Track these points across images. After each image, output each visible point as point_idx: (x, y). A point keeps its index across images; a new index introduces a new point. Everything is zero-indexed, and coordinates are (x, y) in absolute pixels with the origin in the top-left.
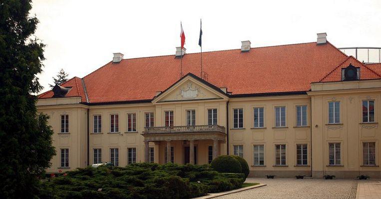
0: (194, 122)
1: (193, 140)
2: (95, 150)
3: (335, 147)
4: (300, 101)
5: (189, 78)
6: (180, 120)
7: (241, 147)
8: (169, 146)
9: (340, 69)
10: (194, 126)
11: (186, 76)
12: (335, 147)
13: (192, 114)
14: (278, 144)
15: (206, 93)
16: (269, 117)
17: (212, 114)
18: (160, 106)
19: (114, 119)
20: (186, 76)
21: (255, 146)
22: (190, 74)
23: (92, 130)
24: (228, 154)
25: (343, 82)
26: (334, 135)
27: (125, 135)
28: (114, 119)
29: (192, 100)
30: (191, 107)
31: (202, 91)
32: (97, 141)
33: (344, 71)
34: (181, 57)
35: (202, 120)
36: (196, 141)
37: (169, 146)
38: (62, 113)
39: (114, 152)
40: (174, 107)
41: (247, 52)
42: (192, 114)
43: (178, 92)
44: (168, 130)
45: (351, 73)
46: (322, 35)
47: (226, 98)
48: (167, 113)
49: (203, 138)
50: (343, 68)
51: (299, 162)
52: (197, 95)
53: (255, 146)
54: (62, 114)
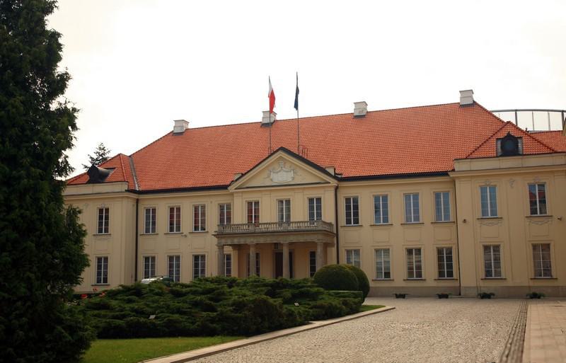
2: (147, 259)
3: (492, 252)
4: (439, 185)
5: (281, 154)
6: (268, 214)
7: (357, 252)
8: (252, 252)
9: (493, 140)
11: (277, 151)
15: (305, 175)
17: (315, 205)
19: (174, 213)
20: (277, 151)
21: (377, 251)
22: (282, 149)
23: (142, 229)
24: (338, 262)
25: (501, 158)
26: (490, 233)
27: (189, 236)
28: (174, 213)
30: (284, 195)
32: (149, 245)
33: (499, 142)
35: (300, 213)
37: (252, 252)
38: (100, 205)
39: (174, 261)
41: (362, 117)
42: (285, 205)
44: (252, 228)
45: (509, 145)
46: (467, 93)
47: (334, 182)
48: (250, 204)
49: (301, 239)
50: (497, 139)
52: (293, 178)
53: (377, 251)
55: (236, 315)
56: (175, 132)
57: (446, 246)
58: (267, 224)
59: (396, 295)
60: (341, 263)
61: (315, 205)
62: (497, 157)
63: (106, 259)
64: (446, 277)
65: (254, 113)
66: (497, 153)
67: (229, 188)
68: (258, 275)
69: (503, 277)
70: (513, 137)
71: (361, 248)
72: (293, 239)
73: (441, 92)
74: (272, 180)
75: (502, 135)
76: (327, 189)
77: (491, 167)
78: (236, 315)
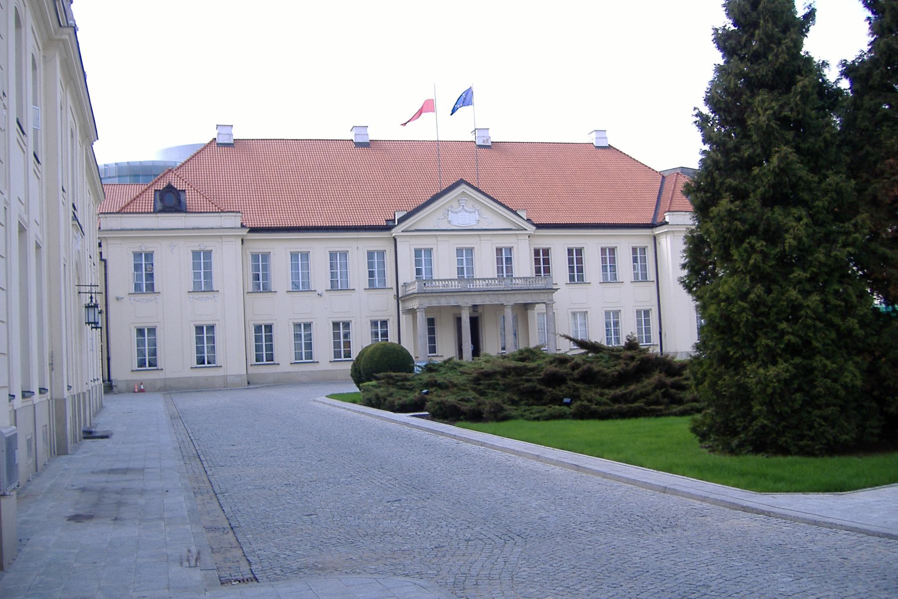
0: (471, 270)
1: (512, 303)
3: (205, 333)
4: (640, 238)
6: (445, 268)
12: (205, 333)
13: (466, 254)
14: (259, 323)
15: (493, 218)
16: (280, 271)
17: (504, 258)
18: (408, 239)
19: (576, 257)
21: (574, 314)
25: (159, 215)
26: (205, 310)
27: (325, 293)
28: (576, 257)
29: (469, 230)
30: (465, 242)
31: (487, 214)
33: (158, 194)
35: (485, 267)
38: (137, 246)
40: (477, 239)
42: (466, 254)
44: (540, 284)
45: (171, 200)
46: (601, 132)
48: (137, 255)
49: (444, 302)
50: (156, 191)
51: (298, 356)
53: (574, 314)
55: (542, 387)
57: (148, 325)
58: (445, 280)
59: (10, 401)
61: (504, 258)
62: (154, 212)
63: (269, 328)
64: (147, 367)
66: (154, 209)
67: (393, 230)
68: (433, 350)
70: (176, 189)
75: (161, 186)
76: (439, 239)
77: (210, 225)
78: (542, 387)
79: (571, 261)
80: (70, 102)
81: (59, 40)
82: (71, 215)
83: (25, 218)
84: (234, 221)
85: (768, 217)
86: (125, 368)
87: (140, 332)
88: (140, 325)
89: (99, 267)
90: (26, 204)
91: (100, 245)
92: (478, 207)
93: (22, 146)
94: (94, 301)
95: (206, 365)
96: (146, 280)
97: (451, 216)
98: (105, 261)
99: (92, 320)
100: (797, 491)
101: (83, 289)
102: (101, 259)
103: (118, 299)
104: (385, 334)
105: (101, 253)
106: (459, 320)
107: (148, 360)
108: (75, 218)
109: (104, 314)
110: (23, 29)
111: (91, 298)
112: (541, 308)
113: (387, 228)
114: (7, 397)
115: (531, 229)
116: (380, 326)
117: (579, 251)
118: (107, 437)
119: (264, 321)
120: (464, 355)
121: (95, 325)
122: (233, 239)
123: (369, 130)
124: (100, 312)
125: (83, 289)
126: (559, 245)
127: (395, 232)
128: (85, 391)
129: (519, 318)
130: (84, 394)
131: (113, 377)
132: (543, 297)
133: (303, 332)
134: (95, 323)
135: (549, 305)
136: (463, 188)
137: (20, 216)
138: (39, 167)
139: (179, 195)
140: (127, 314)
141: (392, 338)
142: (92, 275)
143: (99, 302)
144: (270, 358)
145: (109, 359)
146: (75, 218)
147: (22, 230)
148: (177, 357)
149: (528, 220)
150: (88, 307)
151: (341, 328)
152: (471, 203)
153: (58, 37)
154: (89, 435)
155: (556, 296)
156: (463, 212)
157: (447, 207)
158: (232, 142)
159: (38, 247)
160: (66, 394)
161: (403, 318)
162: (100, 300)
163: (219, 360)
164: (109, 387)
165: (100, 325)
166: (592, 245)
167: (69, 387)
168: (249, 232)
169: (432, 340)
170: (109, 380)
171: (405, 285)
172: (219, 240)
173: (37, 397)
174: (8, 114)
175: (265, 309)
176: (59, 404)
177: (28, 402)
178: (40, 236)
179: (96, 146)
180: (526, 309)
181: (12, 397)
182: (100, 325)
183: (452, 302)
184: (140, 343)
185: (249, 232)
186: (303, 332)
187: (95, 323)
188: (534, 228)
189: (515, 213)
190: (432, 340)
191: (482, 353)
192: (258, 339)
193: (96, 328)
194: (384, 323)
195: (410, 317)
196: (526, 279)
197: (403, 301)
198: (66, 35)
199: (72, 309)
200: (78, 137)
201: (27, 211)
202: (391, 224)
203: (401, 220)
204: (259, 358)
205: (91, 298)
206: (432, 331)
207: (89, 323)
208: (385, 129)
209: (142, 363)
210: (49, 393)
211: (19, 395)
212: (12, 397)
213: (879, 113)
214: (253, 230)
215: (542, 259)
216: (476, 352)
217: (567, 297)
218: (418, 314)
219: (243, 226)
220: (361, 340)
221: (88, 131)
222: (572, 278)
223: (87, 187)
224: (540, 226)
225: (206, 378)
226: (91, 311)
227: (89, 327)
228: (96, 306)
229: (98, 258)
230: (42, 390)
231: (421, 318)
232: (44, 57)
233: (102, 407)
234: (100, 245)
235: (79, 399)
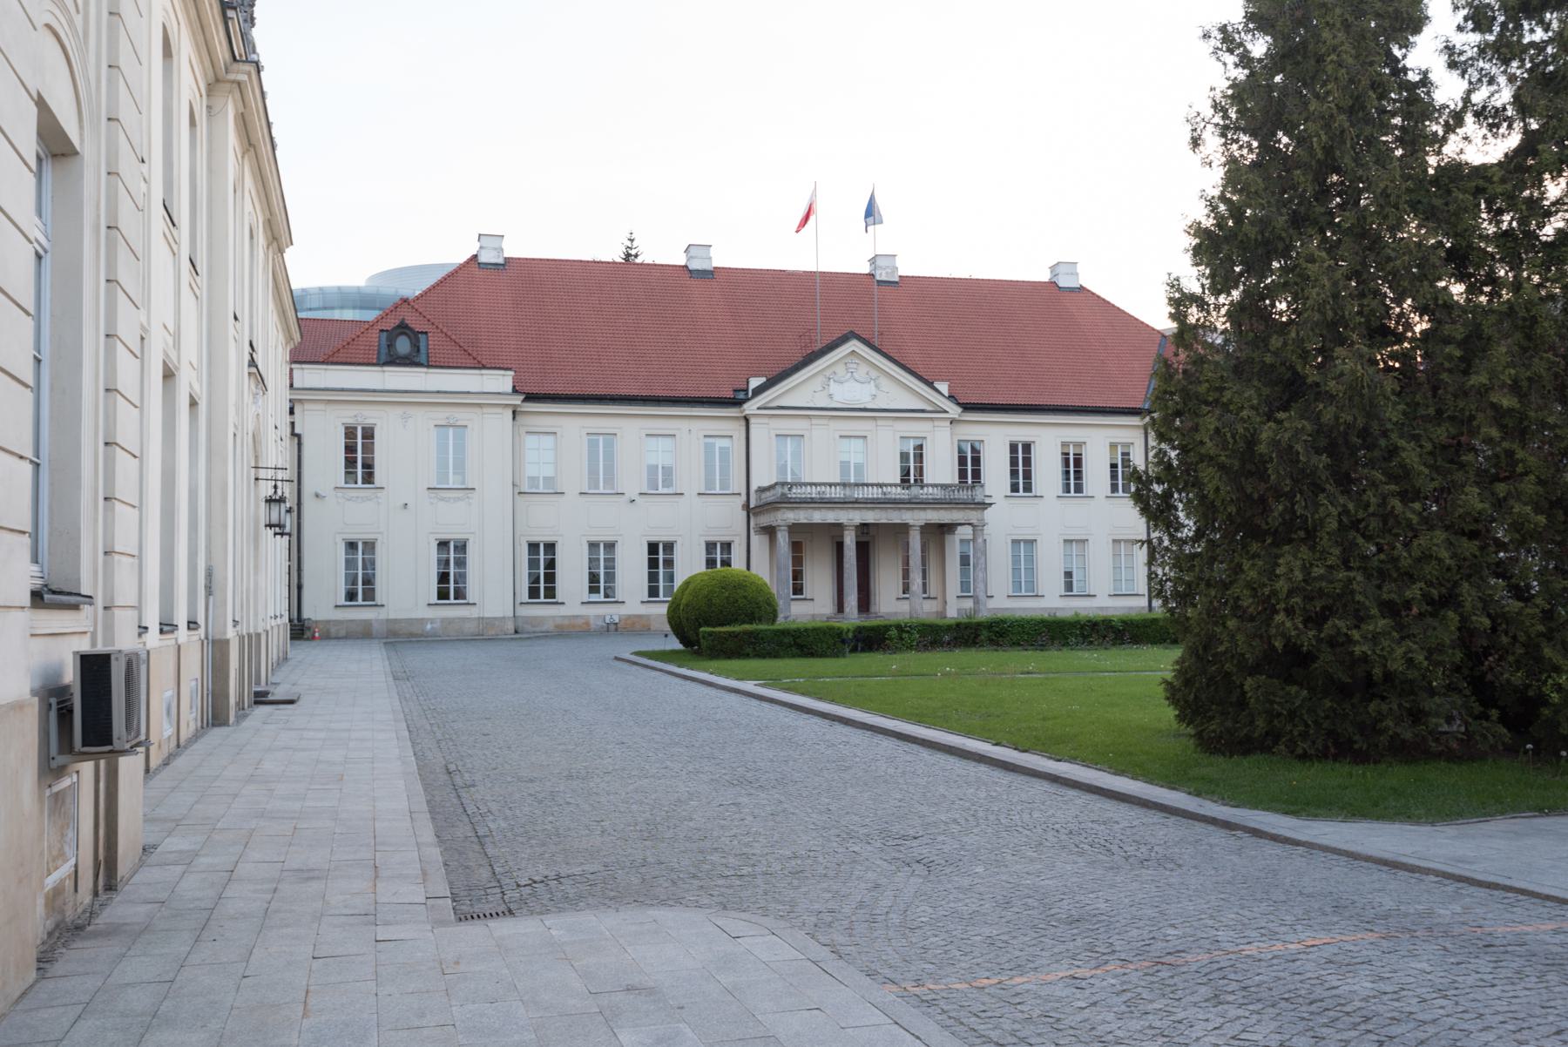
0: (920, 471)
3: (361, 553)
8: (850, 540)
9: (375, 334)
10: (919, 481)
12: (361, 553)
15: (896, 390)
16: (1048, 470)
19: (1021, 457)
20: (843, 340)
24: (748, 568)
26: (453, 520)
27: (639, 500)
28: (1021, 457)
31: (885, 383)
34: (1053, 284)
36: (864, 528)
37: (850, 540)
38: (350, 415)
41: (628, 273)
43: (817, 383)
44: (964, 495)
54: (350, 421)
56: (482, 259)
59: (140, 635)
60: (754, 570)
65: (1044, 276)
67: (745, 406)
69: (619, 597)
71: (379, 537)
72: (870, 517)
73: (1024, 264)
74: (830, 396)
76: (814, 421)
79: (1014, 462)
80: (249, 182)
81: (233, 82)
82: (247, 358)
83: (173, 355)
84: (501, 381)
85: (1275, 443)
86: (323, 603)
87: (352, 546)
88: (352, 537)
89: (288, 444)
90: (177, 337)
91: (292, 412)
92: (874, 374)
93: (172, 245)
94: (279, 492)
95: (452, 600)
96: (359, 458)
97: (834, 388)
98: (299, 436)
99: (275, 520)
100: (1380, 817)
101: (262, 474)
102: (293, 434)
103: (317, 496)
104: (727, 563)
105: (293, 424)
106: (840, 546)
107: (361, 588)
108: (252, 363)
109: (295, 514)
110: (175, 58)
111: (275, 487)
112: (964, 532)
113: (736, 403)
114: (136, 631)
115: (954, 411)
116: (717, 552)
117: (1027, 447)
118: (291, 702)
119: (542, 537)
120: (847, 610)
121: (277, 528)
122: (499, 410)
123: (712, 252)
124: (289, 511)
125: (262, 474)
126: (995, 438)
127: (750, 408)
128: (260, 630)
129: (932, 546)
130: (258, 635)
131: (305, 615)
132: (972, 516)
133: (602, 556)
134: (279, 526)
135: (977, 528)
136: (854, 345)
137: (166, 354)
138: (198, 279)
139: (418, 340)
140: (335, 514)
141: (738, 563)
142: (277, 453)
143: (287, 495)
144: (550, 592)
145: (300, 587)
146: (252, 363)
147: (169, 375)
148: (406, 589)
149: (951, 397)
150: (269, 501)
151: (658, 554)
152: (864, 368)
153: (231, 77)
154: (261, 699)
155: (988, 513)
156: (851, 378)
157: (828, 373)
158: (501, 261)
159: (193, 403)
160: (231, 633)
161: (755, 538)
162: (287, 490)
163: (472, 593)
164: (300, 630)
165: (287, 530)
166: (1048, 440)
167: (235, 623)
168: (525, 400)
169: (797, 575)
170: (299, 618)
171: (761, 490)
172: (478, 410)
173: (183, 634)
174: (149, 189)
175: (543, 522)
176: (217, 650)
177: (169, 640)
178: (196, 387)
179: (289, 254)
180: (943, 533)
181: (143, 629)
182: (287, 530)
183: (830, 516)
184: (350, 564)
185: (525, 400)
186: (602, 556)
187: (279, 526)
188: (959, 410)
189: (930, 384)
190: (797, 575)
191: (873, 609)
192: (533, 564)
193: (282, 534)
194: (727, 546)
195: (765, 539)
196: (944, 487)
197: (756, 514)
198: (241, 73)
199: (243, 505)
200: (261, 240)
201: (177, 344)
202: (741, 396)
203: (759, 391)
204: (534, 593)
205: (275, 487)
206: (797, 561)
207: (270, 526)
208: (735, 251)
209: (351, 596)
210: (202, 631)
211: (154, 628)
212: (143, 629)
213: (1417, 319)
214: (530, 398)
215: (970, 464)
216: (865, 603)
217: (1005, 517)
218: (779, 535)
219: (515, 391)
220: (689, 565)
221: (277, 234)
222: (1015, 488)
223: (275, 317)
224: (968, 407)
225: (450, 621)
226: (275, 508)
227: (270, 532)
228: (282, 500)
229: (289, 430)
230: (192, 624)
231: (783, 539)
232: (209, 107)
233: (286, 659)
234: (292, 412)
235: (252, 642)
